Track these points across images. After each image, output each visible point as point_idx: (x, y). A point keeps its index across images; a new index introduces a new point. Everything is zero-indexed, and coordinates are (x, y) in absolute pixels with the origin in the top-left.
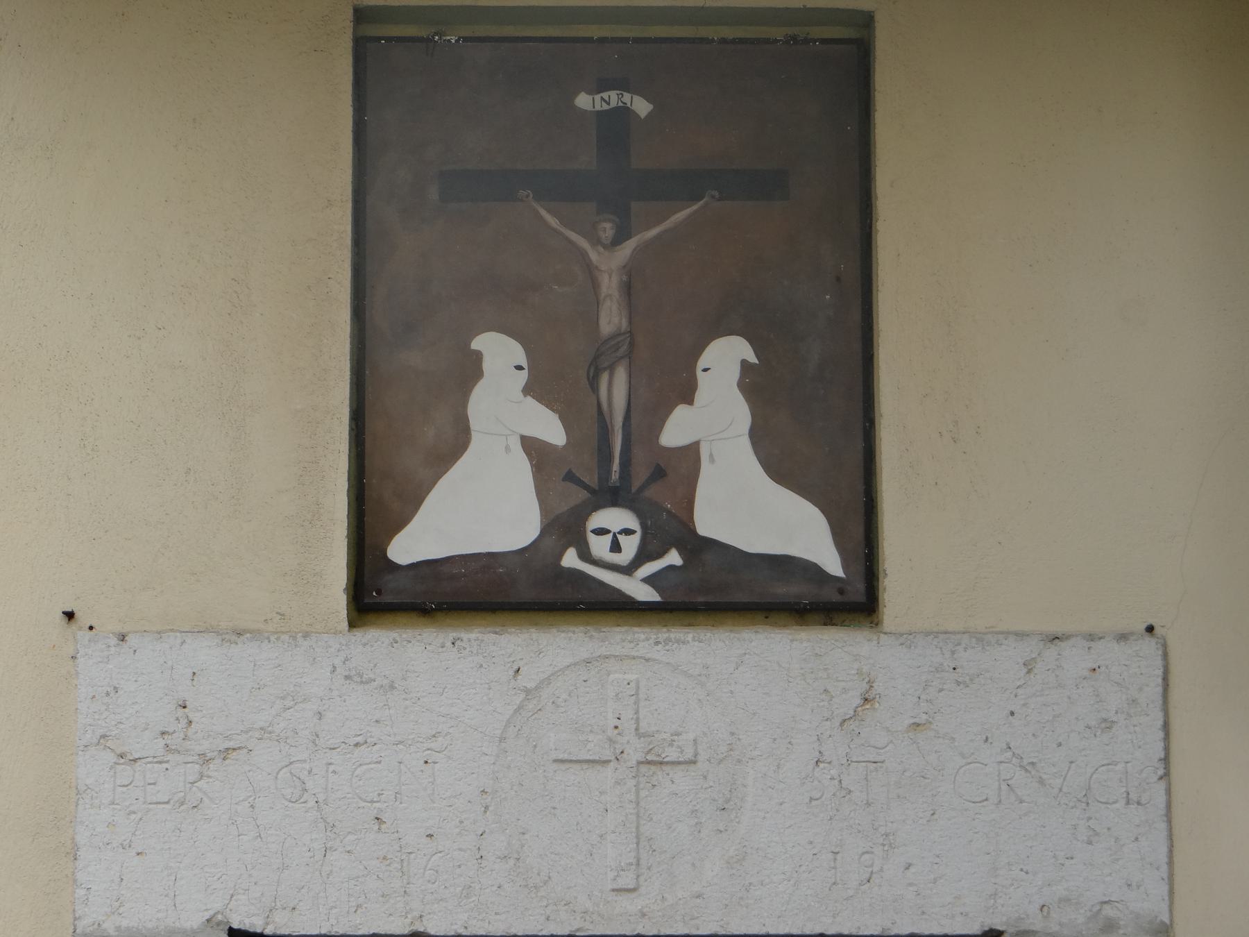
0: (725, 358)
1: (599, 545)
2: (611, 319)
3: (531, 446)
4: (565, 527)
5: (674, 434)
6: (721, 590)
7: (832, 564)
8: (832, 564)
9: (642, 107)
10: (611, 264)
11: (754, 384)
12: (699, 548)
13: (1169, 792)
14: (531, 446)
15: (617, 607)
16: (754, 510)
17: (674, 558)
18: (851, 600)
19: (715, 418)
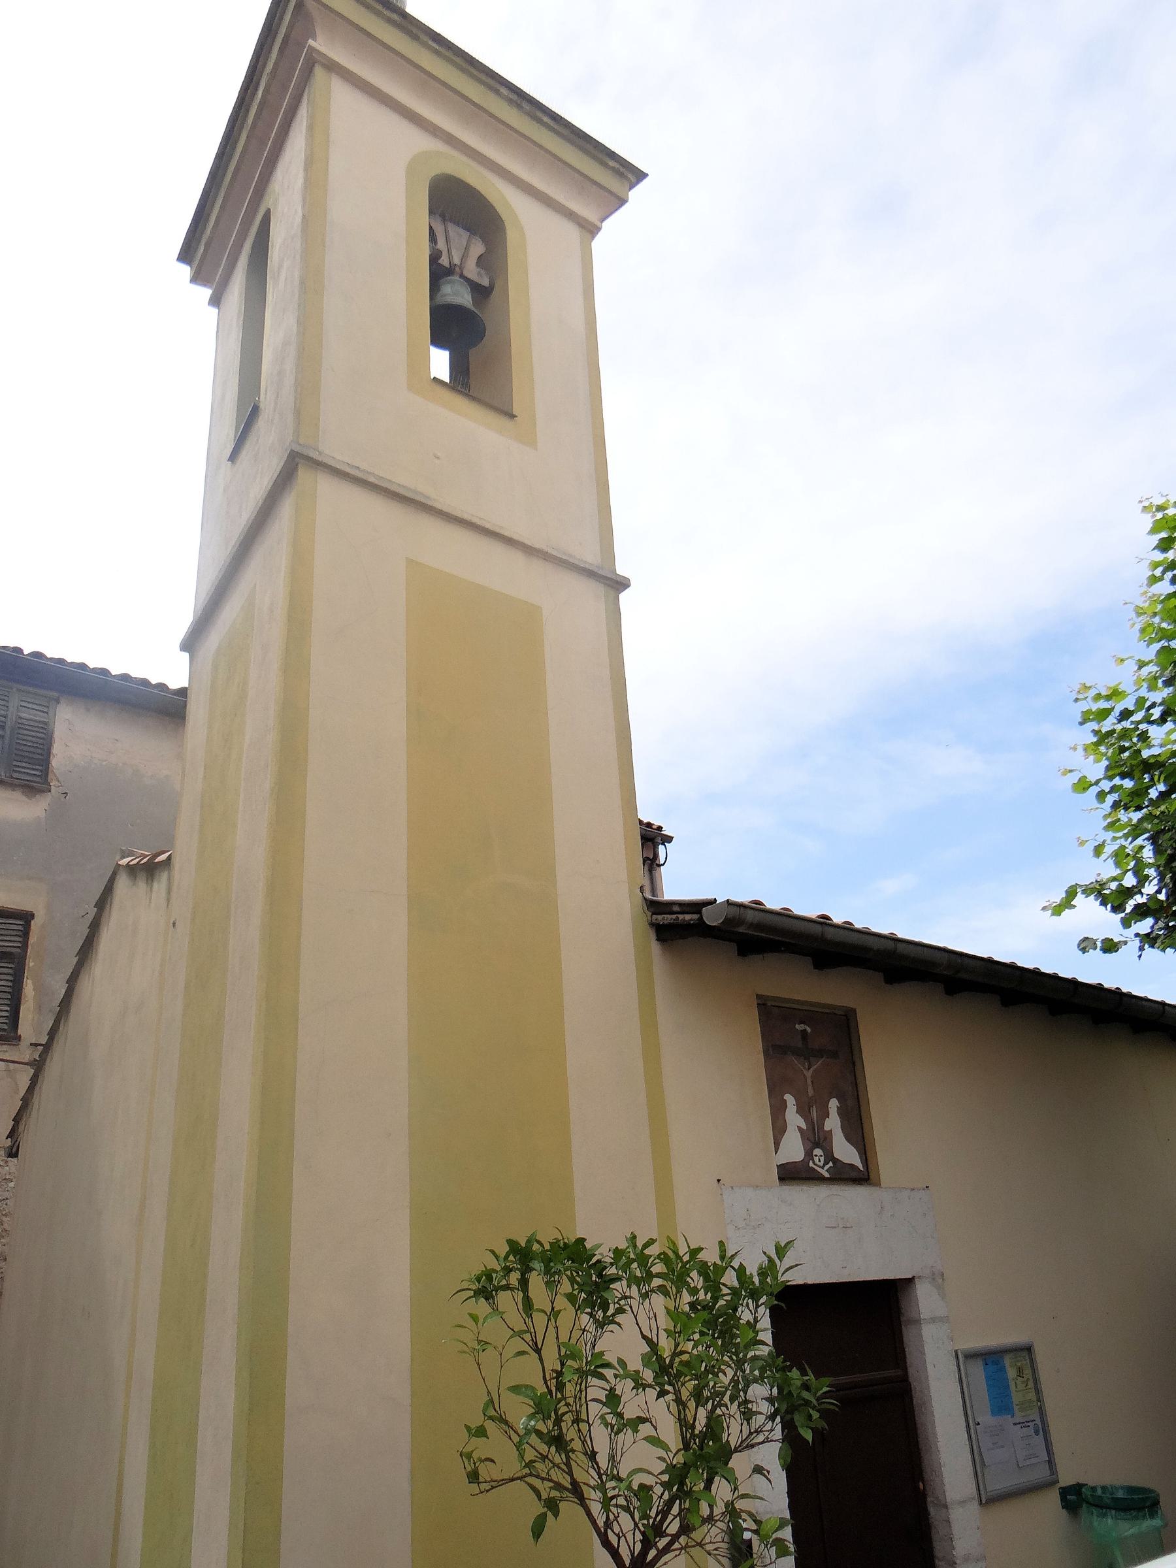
0: (834, 1104)
1: (816, 1159)
2: (811, 1092)
3: (800, 1128)
4: (809, 1155)
5: (827, 1128)
6: (844, 1176)
7: (859, 1164)
8: (859, 1164)
9: (809, 1030)
10: (809, 1074)
11: (842, 1112)
12: (836, 1161)
13: (34, 1081)
14: (800, 1128)
15: (820, 1179)
16: (845, 1152)
17: (831, 1164)
18: (862, 1177)
19: (833, 1123)
